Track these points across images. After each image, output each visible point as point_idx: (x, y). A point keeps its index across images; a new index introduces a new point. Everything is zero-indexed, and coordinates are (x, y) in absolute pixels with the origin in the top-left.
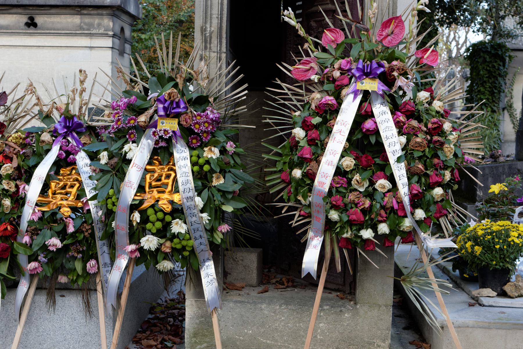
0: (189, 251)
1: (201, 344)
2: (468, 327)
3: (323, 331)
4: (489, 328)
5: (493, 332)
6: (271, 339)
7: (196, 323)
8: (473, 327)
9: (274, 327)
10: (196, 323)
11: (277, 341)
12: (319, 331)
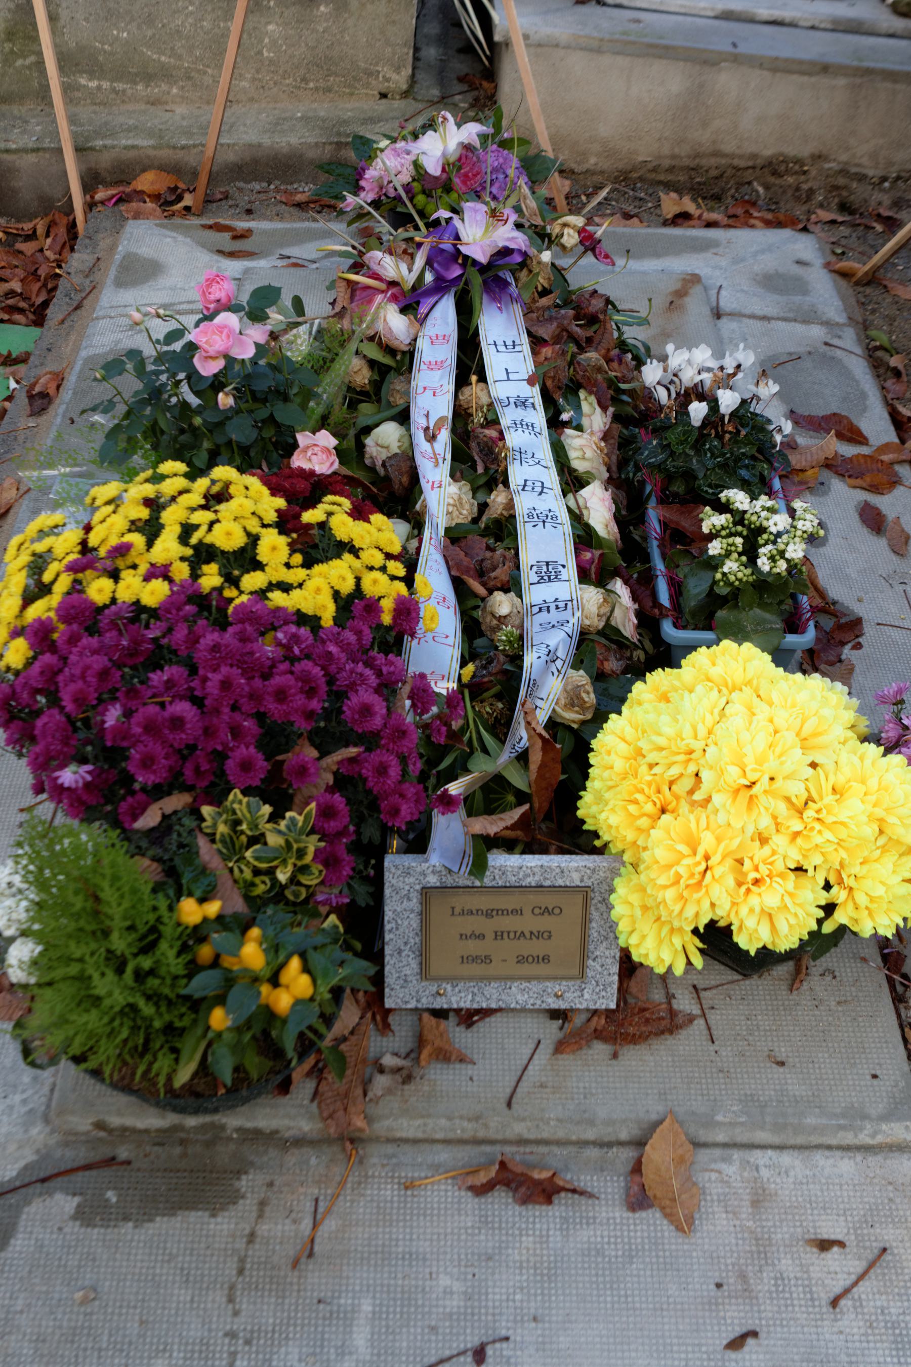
0: (11, 940)
1: (25, 57)
2: (557, 46)
3: (274, 42)
4: (599, 51)
5: (606, 60)
6: (168, 52)
7: (9, 10)
8: (567, 47)
9: (172, 26)
10: (9, 10)
11: (180, 57)
12: (267, 40)
